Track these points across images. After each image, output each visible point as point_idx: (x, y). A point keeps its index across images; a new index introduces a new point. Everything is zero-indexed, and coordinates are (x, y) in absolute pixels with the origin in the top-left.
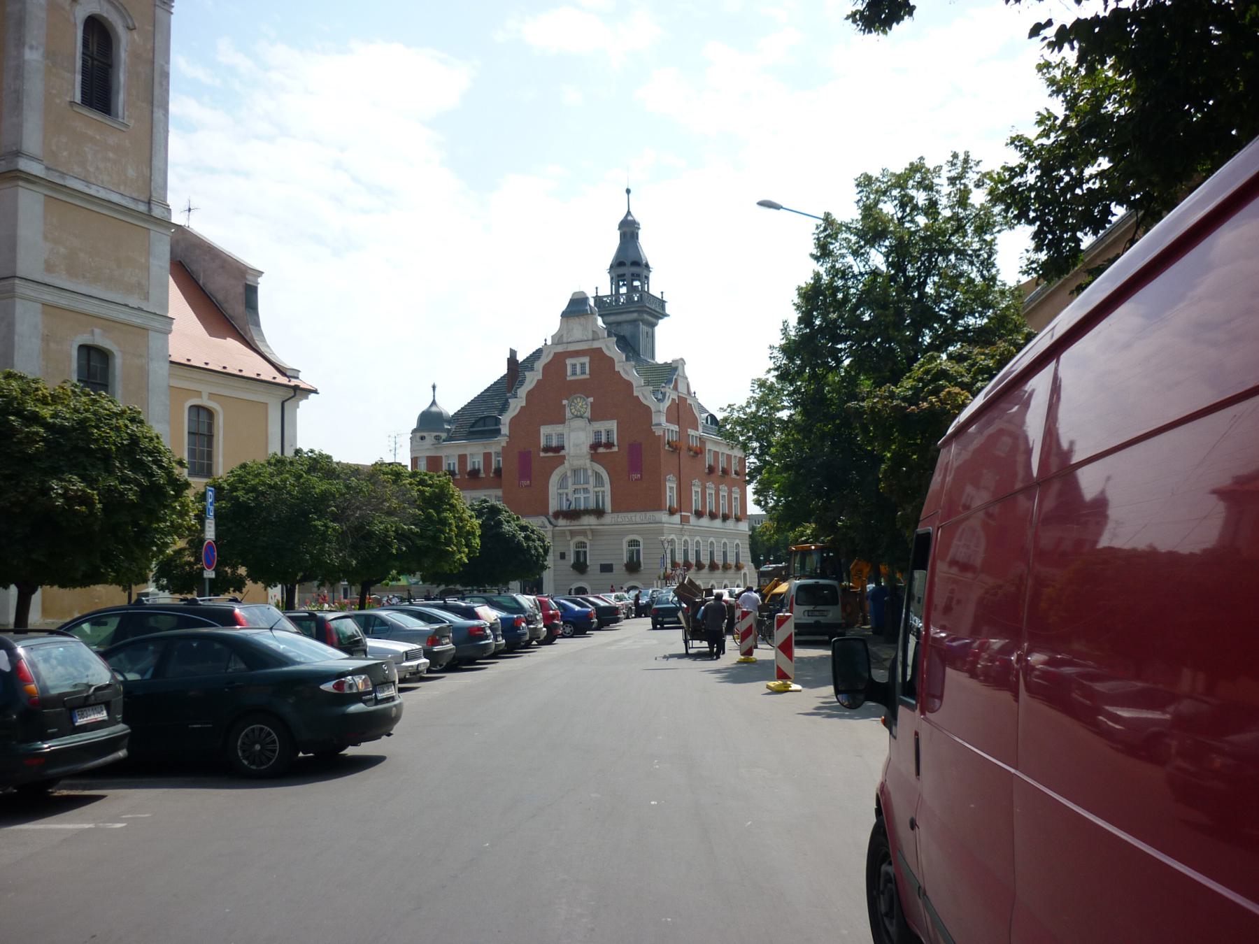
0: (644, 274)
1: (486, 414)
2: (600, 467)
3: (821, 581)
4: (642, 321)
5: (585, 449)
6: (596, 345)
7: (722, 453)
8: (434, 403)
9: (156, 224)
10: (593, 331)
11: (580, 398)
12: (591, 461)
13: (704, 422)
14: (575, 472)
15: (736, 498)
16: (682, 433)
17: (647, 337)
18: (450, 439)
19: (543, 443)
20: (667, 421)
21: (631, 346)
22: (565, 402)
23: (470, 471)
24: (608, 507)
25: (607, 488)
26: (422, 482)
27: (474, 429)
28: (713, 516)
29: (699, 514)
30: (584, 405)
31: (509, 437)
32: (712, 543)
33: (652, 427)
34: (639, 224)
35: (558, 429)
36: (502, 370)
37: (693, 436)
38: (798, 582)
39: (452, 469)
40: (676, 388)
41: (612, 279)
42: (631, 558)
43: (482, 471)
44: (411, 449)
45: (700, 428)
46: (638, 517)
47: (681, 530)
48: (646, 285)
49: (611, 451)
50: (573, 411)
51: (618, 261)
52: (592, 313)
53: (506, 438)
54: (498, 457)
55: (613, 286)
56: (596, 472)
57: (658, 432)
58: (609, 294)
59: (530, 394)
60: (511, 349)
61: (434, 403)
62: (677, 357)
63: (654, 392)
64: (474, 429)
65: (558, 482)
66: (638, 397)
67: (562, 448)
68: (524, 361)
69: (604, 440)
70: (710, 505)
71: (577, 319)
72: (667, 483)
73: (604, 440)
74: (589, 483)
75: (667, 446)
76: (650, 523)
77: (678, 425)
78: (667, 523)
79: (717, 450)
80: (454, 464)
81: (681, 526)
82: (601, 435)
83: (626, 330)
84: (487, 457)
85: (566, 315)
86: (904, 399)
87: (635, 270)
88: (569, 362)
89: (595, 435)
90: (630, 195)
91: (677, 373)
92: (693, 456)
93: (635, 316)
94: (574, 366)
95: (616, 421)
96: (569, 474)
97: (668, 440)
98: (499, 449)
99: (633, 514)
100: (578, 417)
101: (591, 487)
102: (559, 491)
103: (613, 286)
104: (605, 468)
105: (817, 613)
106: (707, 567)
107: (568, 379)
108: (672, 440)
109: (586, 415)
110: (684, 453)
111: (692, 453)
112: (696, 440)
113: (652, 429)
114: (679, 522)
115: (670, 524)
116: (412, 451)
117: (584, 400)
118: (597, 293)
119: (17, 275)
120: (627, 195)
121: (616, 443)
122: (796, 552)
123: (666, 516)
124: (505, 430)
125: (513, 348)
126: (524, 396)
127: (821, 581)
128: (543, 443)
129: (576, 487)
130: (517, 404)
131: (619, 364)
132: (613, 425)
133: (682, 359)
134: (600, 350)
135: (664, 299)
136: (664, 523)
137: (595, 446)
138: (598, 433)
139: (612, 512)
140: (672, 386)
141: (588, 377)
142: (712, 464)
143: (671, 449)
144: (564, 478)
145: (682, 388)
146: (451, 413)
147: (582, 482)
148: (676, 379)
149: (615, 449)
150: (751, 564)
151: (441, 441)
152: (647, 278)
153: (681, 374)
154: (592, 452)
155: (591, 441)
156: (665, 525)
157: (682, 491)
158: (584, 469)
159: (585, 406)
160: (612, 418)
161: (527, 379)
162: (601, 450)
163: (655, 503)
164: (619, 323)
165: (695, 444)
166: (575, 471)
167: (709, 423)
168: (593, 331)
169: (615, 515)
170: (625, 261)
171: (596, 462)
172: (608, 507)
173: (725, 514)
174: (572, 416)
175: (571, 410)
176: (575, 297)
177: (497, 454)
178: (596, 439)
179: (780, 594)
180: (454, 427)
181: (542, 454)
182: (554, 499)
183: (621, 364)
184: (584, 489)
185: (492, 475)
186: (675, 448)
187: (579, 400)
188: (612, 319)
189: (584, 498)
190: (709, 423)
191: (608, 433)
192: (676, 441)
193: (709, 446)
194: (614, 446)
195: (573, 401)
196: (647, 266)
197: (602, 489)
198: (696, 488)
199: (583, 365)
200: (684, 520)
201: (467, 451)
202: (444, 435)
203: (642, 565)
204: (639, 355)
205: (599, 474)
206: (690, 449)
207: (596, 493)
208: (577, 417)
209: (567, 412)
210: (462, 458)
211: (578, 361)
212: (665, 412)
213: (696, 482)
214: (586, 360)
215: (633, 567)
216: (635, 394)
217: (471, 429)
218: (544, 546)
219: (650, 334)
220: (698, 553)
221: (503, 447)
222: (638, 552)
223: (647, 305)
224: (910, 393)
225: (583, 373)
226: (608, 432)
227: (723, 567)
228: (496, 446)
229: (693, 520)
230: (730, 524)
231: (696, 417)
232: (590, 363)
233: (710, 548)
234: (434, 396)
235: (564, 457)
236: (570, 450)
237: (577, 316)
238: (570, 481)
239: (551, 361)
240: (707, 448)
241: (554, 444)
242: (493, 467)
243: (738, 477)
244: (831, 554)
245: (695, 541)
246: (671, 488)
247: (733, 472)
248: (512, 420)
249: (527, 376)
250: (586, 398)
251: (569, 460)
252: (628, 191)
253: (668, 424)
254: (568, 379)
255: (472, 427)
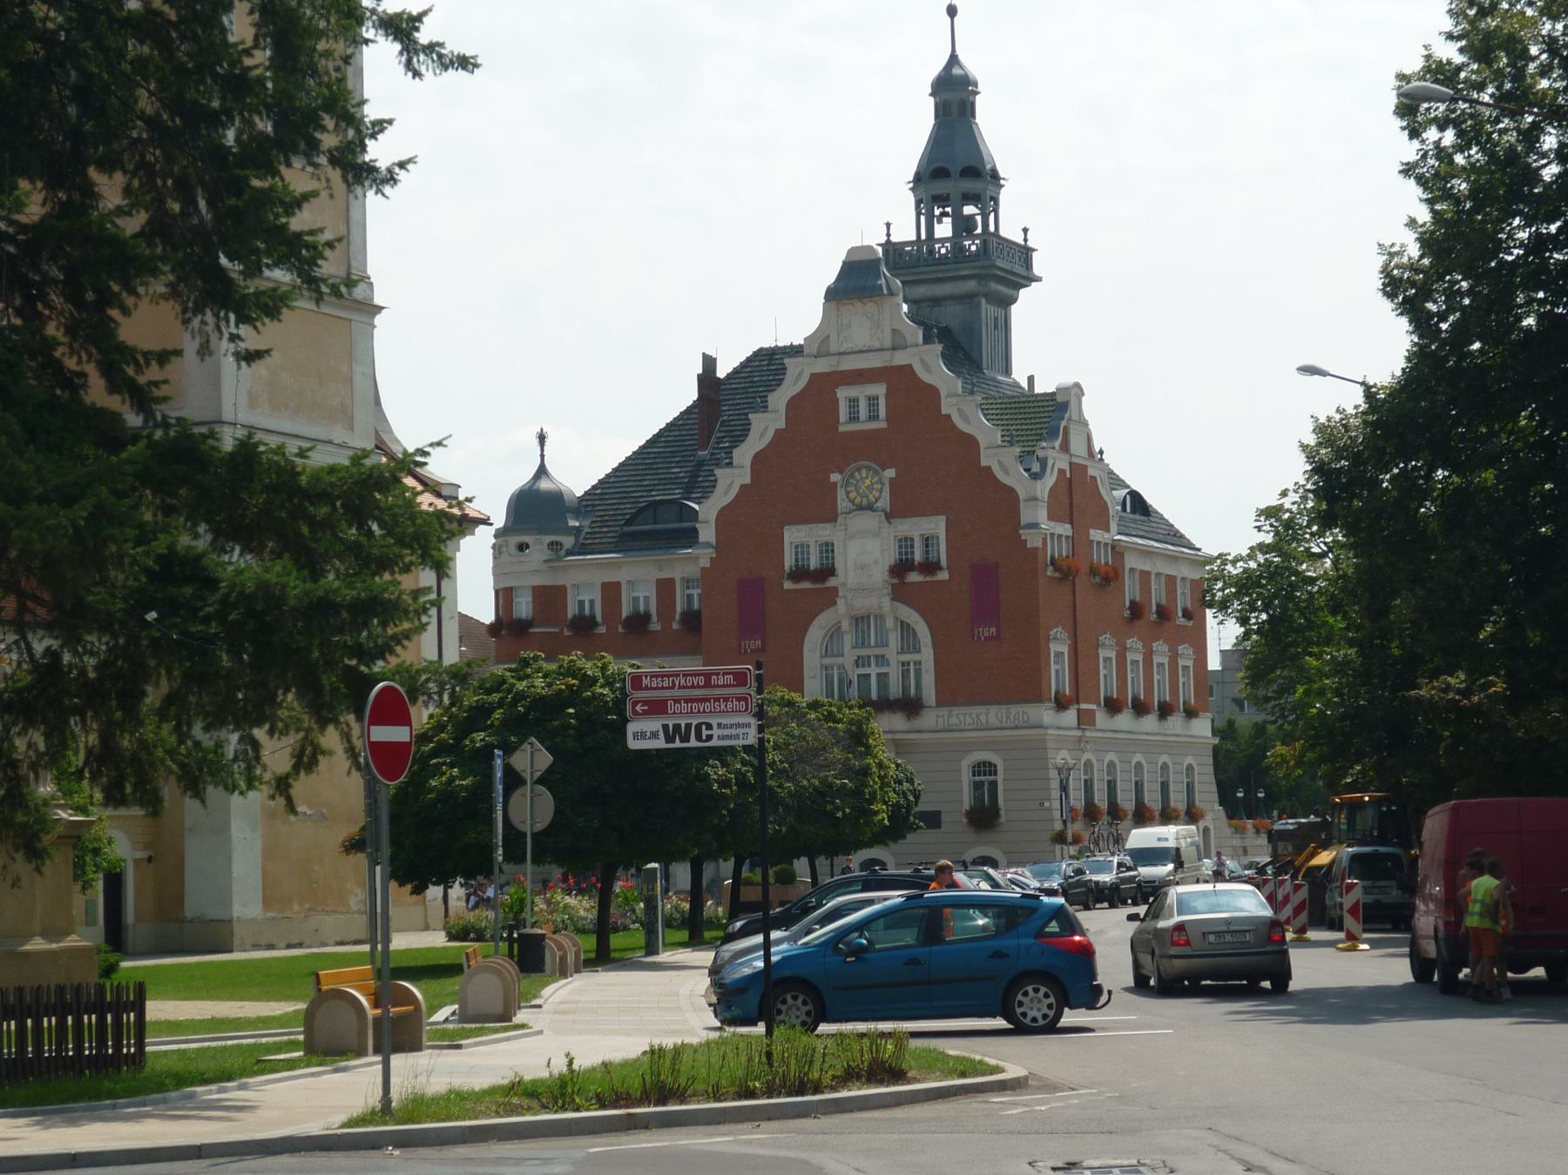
0: (989, 193)
1: (658, 497)
2: (912, 611)
3: (1382, 849)
4: (986, 296)
5: (879, 574)
6: (900, 359)
7: (1158, 574)
8: (542, 471)
9: (359, 310)
10: (894, 331)
11: (868, 468)
12: (893, 599)
13: (1119, 508)
14: (860, 621)
15: (1185, 668)
16: (1078, 540)
17: (996, 328)
18: (582, 549)
19: (789, 561)
20: (1051, 518)
21: (963, 349)
22: (835, 477)
23: (628, 618)
24: (929, 693)
25: (927, 655)
26: (830, 717)
27: (633, 528)
28: (1140, 708)
29: (1113, 706)
30: (876, 483)
31: (717, 548)
32: (1139, 766)
33: (1021, 532)
34: (976, 85)
35: (823, 532)
36: (690, 395)
37: (1099, 543)
38: (1350, 850)
39: (587, 612)
40: (1065, 447)
41: (918, 202)
42: (978, 798)
43: (654, 618)
44: (495, 567)
45: (1114, 526)
46: (992, 714)
47: (1080, 740)
48: (992, 215)
49: (934, 579)
50: (851, 495)
51: (931, 169)
52: (891, 294)
53: (711, 550)
54: (688, 588)
55: (923, 218)
56: (902, 622)
57: (1033, 541)
58: (913, 237)
59: (758, 459)
60: (704, 354)
61: (542, 471)
62: (1068, 380)
63: (1021, 458)
64: (633, 528)
65: (822, 644)
66: (989, 468)
67: (827, 571)
68: (736, 371)
69: (918, 557)
70: (1135, 686)
71: (859, 305)
72: (1051, 646)
73: (918, 557)
74: (887, 645)
75: (1051, 568)
76: (1017, 728)
77: (1071, 523)
78: (1051, 727)
79: (1147, 568)
80: (592, 602)
81: (1079, 733)
82: (912, 546)
83: (951, 316)
84: (665, 588)
85: (834, 295)
86: (1459, 692)
87: (969, 185)
88: (843, 394)
89: (900, 547)
90: (955, 19)
91: (1067, 415)
92: (1100, 585)
93: (971, 285)
94: (853, 402)
95: (944, 518)
96: (845, 625)
97: (1053, 557)
98: (692, 571)
99: (981, 709)
100: (866, 509)
101: (892, 651)
102: (826, 661)
103: (923, 218)
104: (923, 615)
105: (1376, 891)
106: (1130, 817)
107: (842, 429)
108: (1060, 555)
109: (879, 504)
110: (1083, 582)
111: (1098, 579)
112: (1106, 553)
113: (1020, 536)
114: (1076, 725)
115: (1059, 728)
116: (498, 572)
117: (876, 473)
118: (888, 235)
119: (224, 419)
120: (949, 19)
121: (944, 562)
122: (1341, 806)
123: (1051, 712)
124: (707, 533)
125: (709, 353)
126: (748, 462)
127: (1382, 849)
128: (789, 561)
129: (864, 652)
130: (731, 481)
131: (949, 400)
132: (937, 526)
133: (1077, 385)
134: (907, 370)
135: (1030, 244)
136: (1047, 728)
137: (900, 569)
138: (906, 543)
139: (938, 705)
140: (1057, 444)
141: (883, 425)
142: (1138, 599)
143: (1057, 575)
144: (835, 634)
145: (1077, 447)
146: (579, 493)
147: (872, 643)
148: (1065, 428)
149: (944, 575)
150: (1217, 807)
151: (563, 552)
152: (996, 200)
153: (1075, 417)
154: (895, 581)
155: (891, 557)
156: (1050, 732)
157: (1081, 659)
158: (876, 616)
159: (879, 486)
160: (935, 512)
161: (753, 428)
162: (914, 577)
163: (1029, 688)
164: (936, 301)
165: (1102, 558)
166: (857, 619)
167: (1128, 510)
168: (894, 331)
169: (944, 711)
170: (947, 166)
171: (901, 602)
172: (929, 693)
173: (1165, 702)
174: (850, 505)
175: (847, 493)
176: (856, 257)
177: (688, 582)
178: (900, 553)
179: (1319, 868)
180: (587, 523)
181: (788, 585)
182: (814, 677)
183: (954, 400)
184: (877, 656)
185: (675, 626)
186: (1065, 572)
187: (864, 472)
188: (922, 291)
189: (879, 675)
190: (1128, 510)
191: (927, 541)
192: (1067, 557)
193: (1131, 562)
194: (940, 568)
195: (852, 476)
196: (995, 176)
197: (916, 657)
198: (1107, 653)
199: (872, 401)
200: (1085, 720)
201: (621, 576)
202: (568, 541)
203: (1002, 813)
204: (979, 368)
205: (908, 625)
206: (1094, 571)
207: (903, 664)
208: (861, 508)
209: (839, 498)
210: (611, 592)
211: (862, 392)
212: (1046, 499)
213: (1106, 638)
214: (880, 390)
215: (984, 817)
216: (984, 462)
217: (626, 529)
218: (915, 790)
219: (1001, 322)
220: (1112, 786)
221: (702, 569)
222: (994, 785)
223: (999, 263)
224: (1464, 685)
225: (873, 417)
226: (927, 539)
227: (1160, 815)
228: (688, 564)
229: (1101, 718)
230: (1176, 722)
231: (1106, 503)
232: (888, 396)
233: (1136, 775)
234: (542, 456)
235: (835, 590)
236: (847, 574)
237: (860, 299)
238: (848, 641)
239: (803, 391)
240: (1128, 566)
241: (814, 563)
242: (679, 609)
243: (1190, 623)
244: (1394, 808)
245: (1106, 762)
246: (1059, 654)
247: (1180, 614)
248: (722, 515)
249: (753, 421)
250: (880, 471)
251: (846, 598)
252: (952, 11)
253: (1052, 524)
254: (842, 429)
255: (629, 522)
